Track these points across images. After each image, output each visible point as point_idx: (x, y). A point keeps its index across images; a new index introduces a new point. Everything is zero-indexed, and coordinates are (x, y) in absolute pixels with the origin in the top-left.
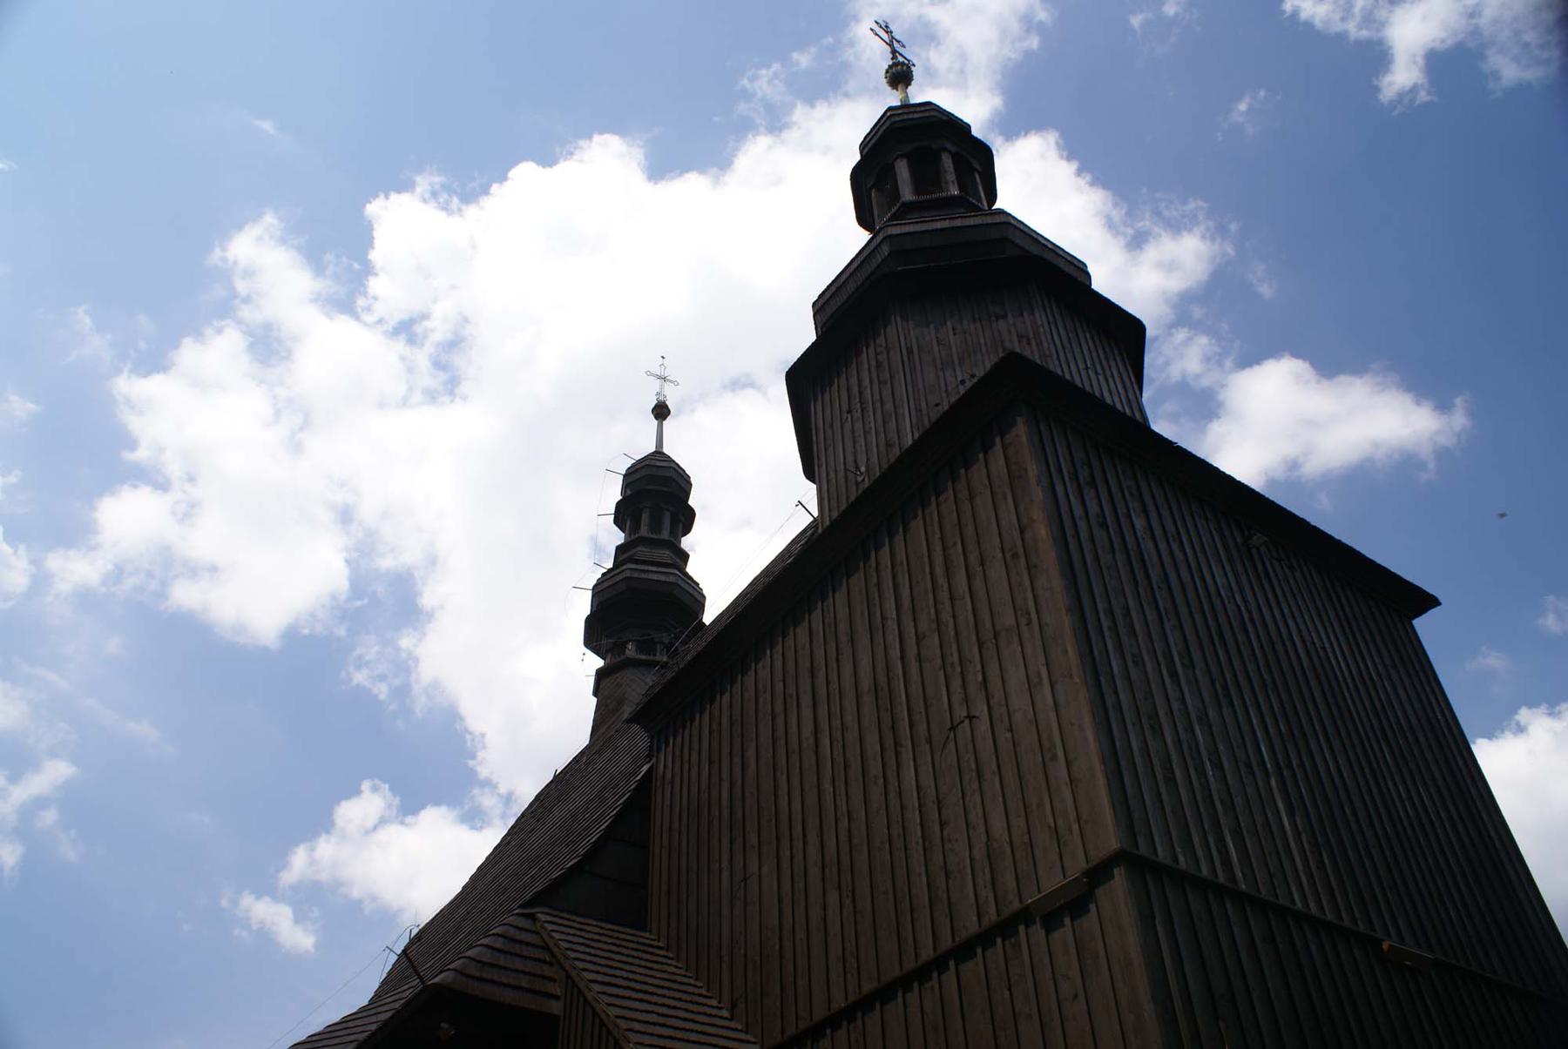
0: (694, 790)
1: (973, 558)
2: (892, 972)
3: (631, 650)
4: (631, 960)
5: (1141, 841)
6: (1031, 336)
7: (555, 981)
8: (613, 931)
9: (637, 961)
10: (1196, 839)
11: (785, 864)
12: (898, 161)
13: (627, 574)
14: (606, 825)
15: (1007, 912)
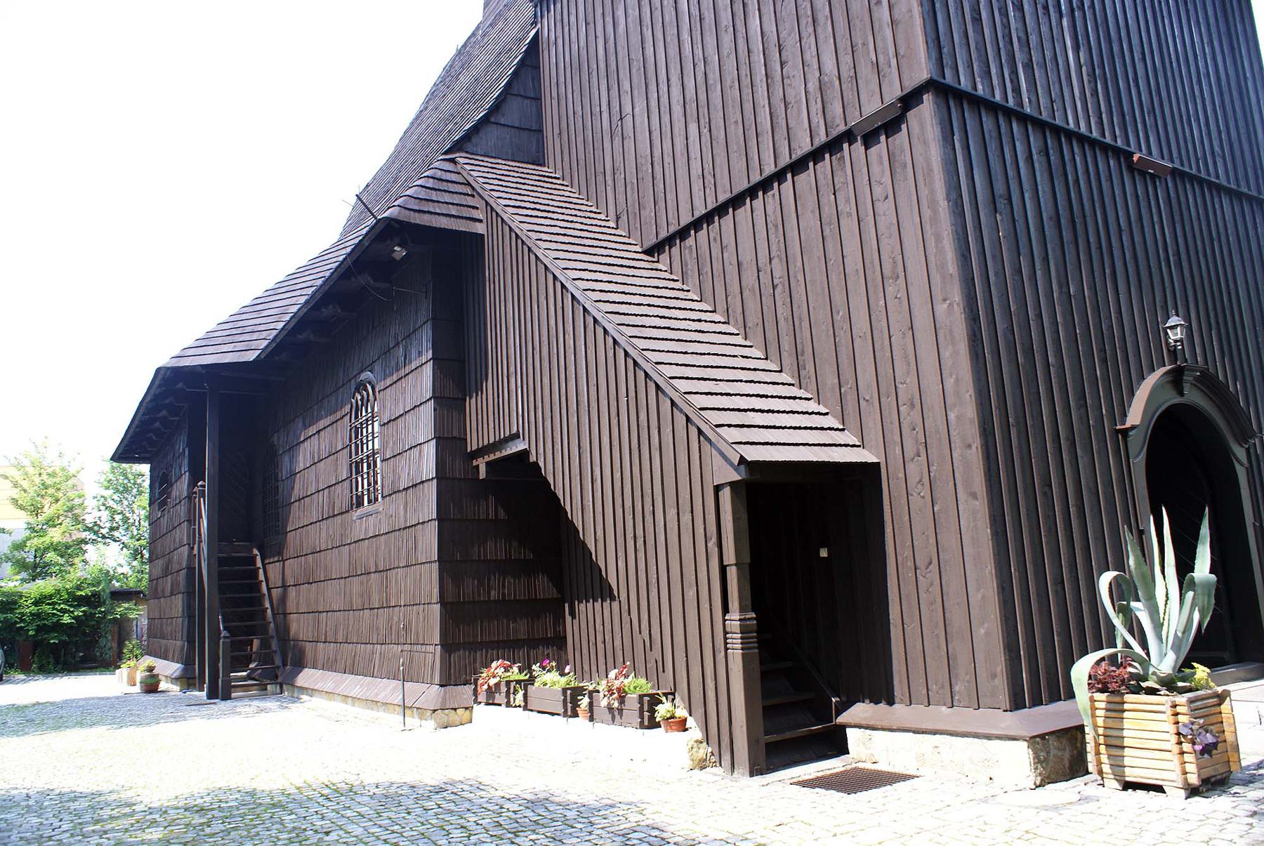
0: (575, 47)
2: (742, 185)
4: (535, 189)
5: (948, 72)
7: (477, 208)
8: (519, 167)
9: (539, 189)
10: (993, 71)
11: (654, 103)
14: (505, 82)
15: (834, 133)
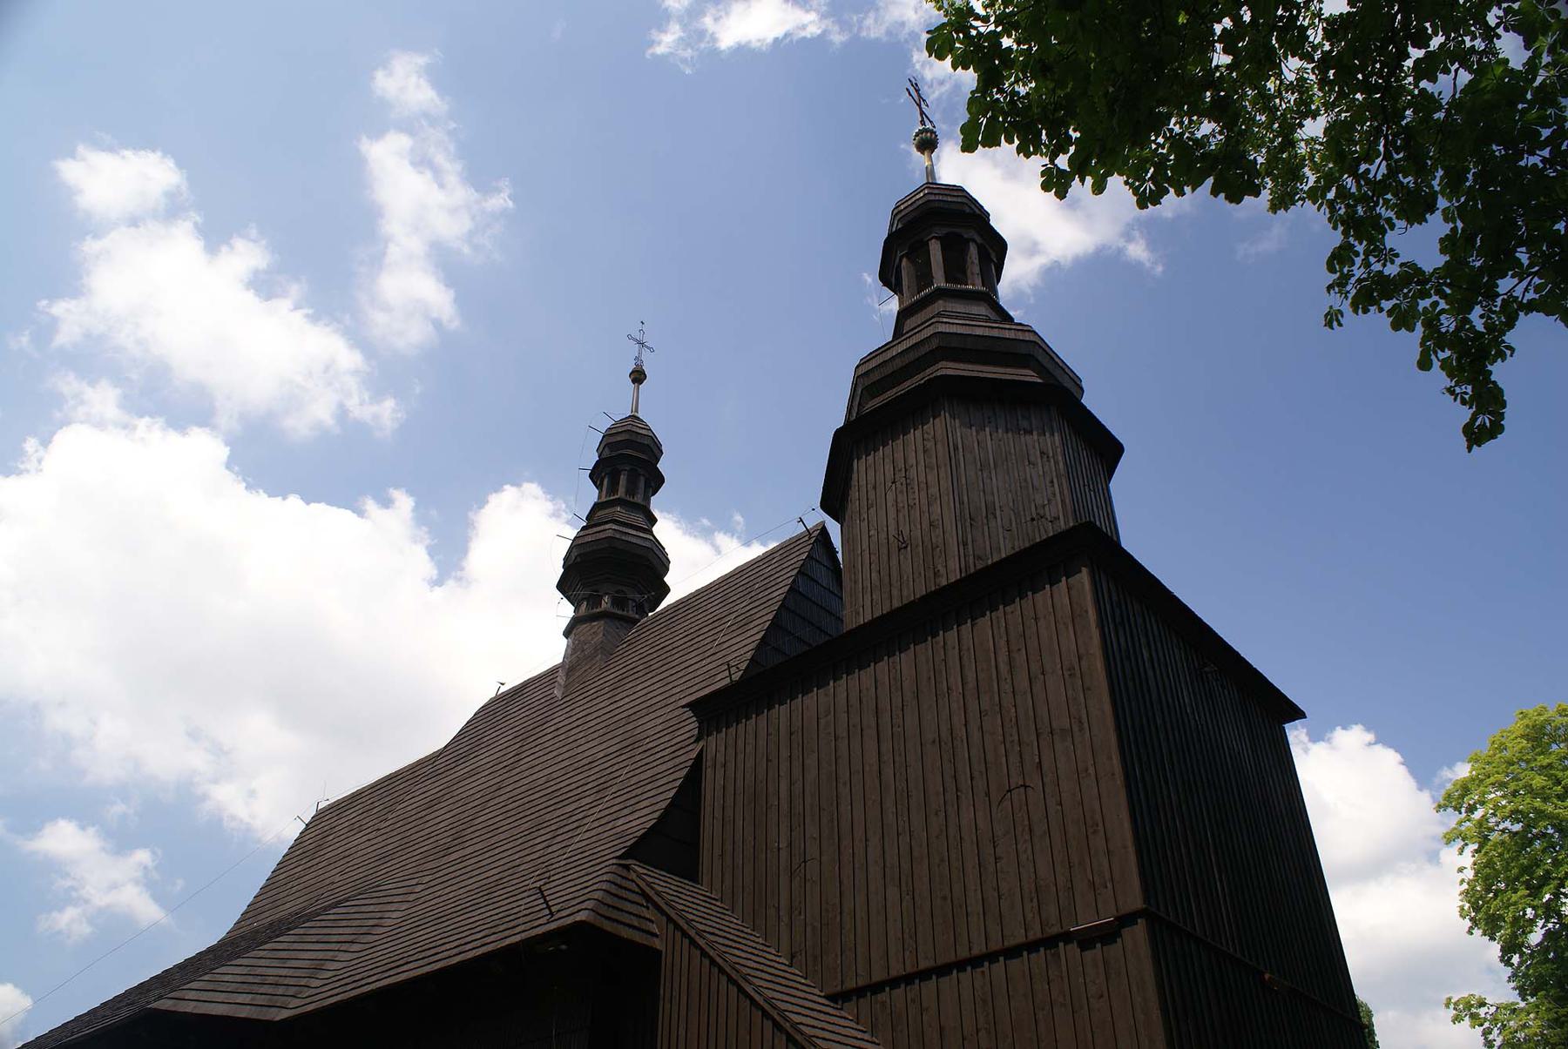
1: (1035, 667)
3: (606, 603)
6: (1051, 455)
12: (933, 241)
13: (609, 534)
